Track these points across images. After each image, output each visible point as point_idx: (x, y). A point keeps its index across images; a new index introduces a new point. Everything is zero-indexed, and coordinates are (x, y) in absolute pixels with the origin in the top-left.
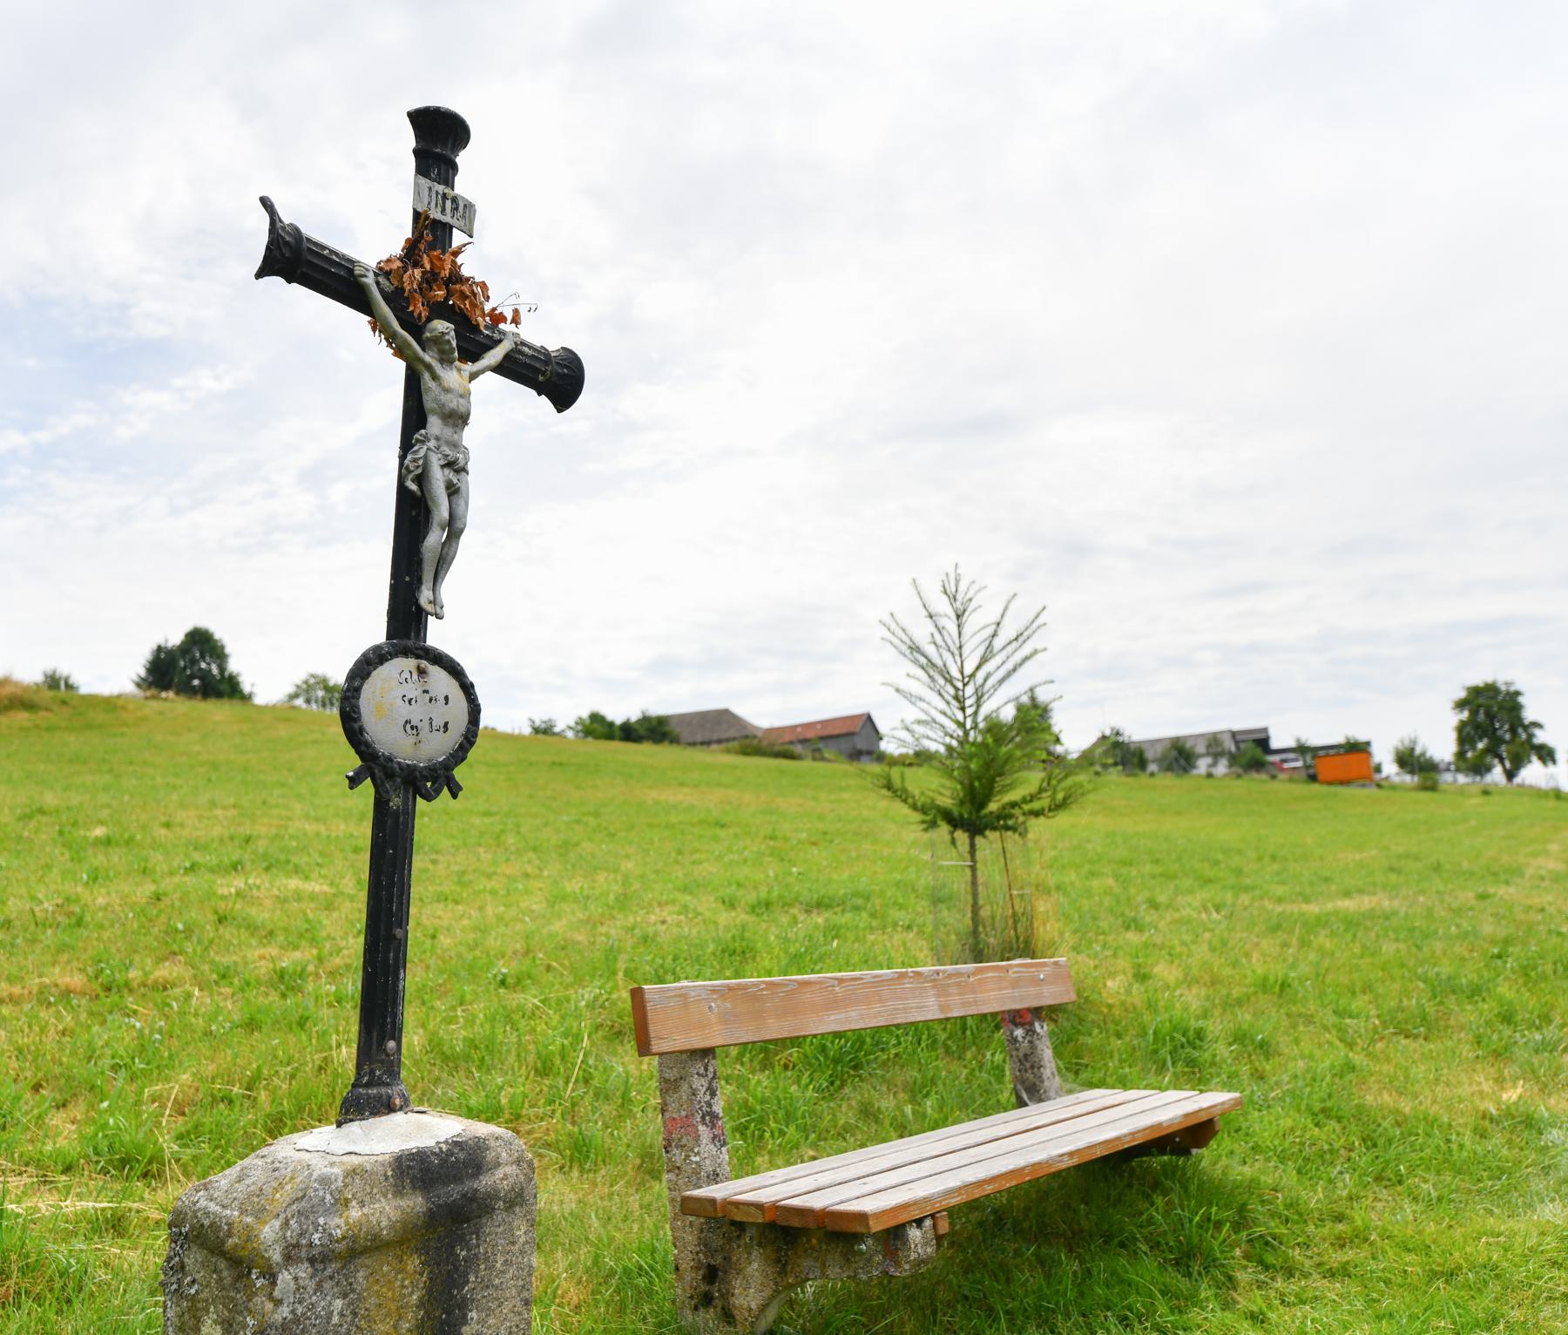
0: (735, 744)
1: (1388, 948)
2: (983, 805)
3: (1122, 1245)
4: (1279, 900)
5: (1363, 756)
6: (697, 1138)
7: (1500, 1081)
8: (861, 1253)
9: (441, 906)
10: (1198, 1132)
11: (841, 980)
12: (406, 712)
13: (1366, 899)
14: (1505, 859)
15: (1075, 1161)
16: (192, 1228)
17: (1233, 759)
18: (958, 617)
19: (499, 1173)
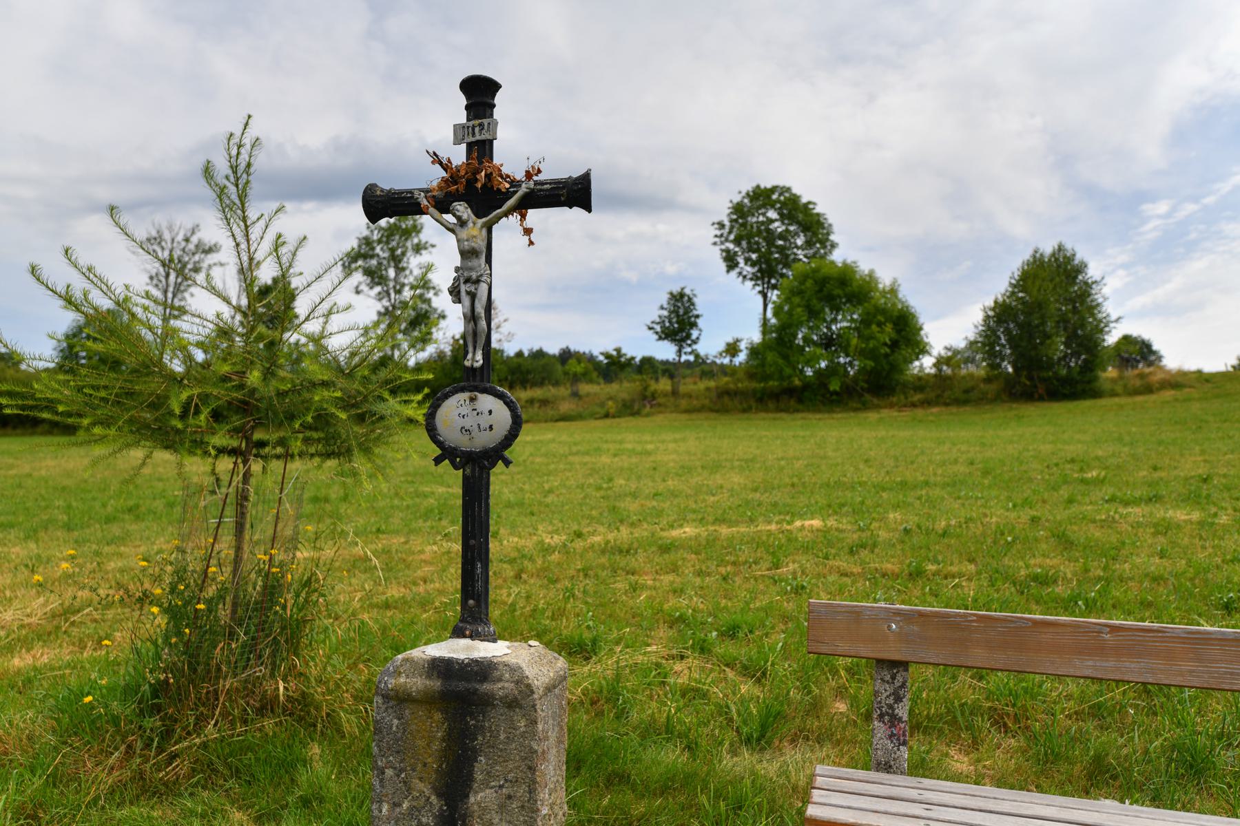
11: (1114, 629)
12: (462, 422)
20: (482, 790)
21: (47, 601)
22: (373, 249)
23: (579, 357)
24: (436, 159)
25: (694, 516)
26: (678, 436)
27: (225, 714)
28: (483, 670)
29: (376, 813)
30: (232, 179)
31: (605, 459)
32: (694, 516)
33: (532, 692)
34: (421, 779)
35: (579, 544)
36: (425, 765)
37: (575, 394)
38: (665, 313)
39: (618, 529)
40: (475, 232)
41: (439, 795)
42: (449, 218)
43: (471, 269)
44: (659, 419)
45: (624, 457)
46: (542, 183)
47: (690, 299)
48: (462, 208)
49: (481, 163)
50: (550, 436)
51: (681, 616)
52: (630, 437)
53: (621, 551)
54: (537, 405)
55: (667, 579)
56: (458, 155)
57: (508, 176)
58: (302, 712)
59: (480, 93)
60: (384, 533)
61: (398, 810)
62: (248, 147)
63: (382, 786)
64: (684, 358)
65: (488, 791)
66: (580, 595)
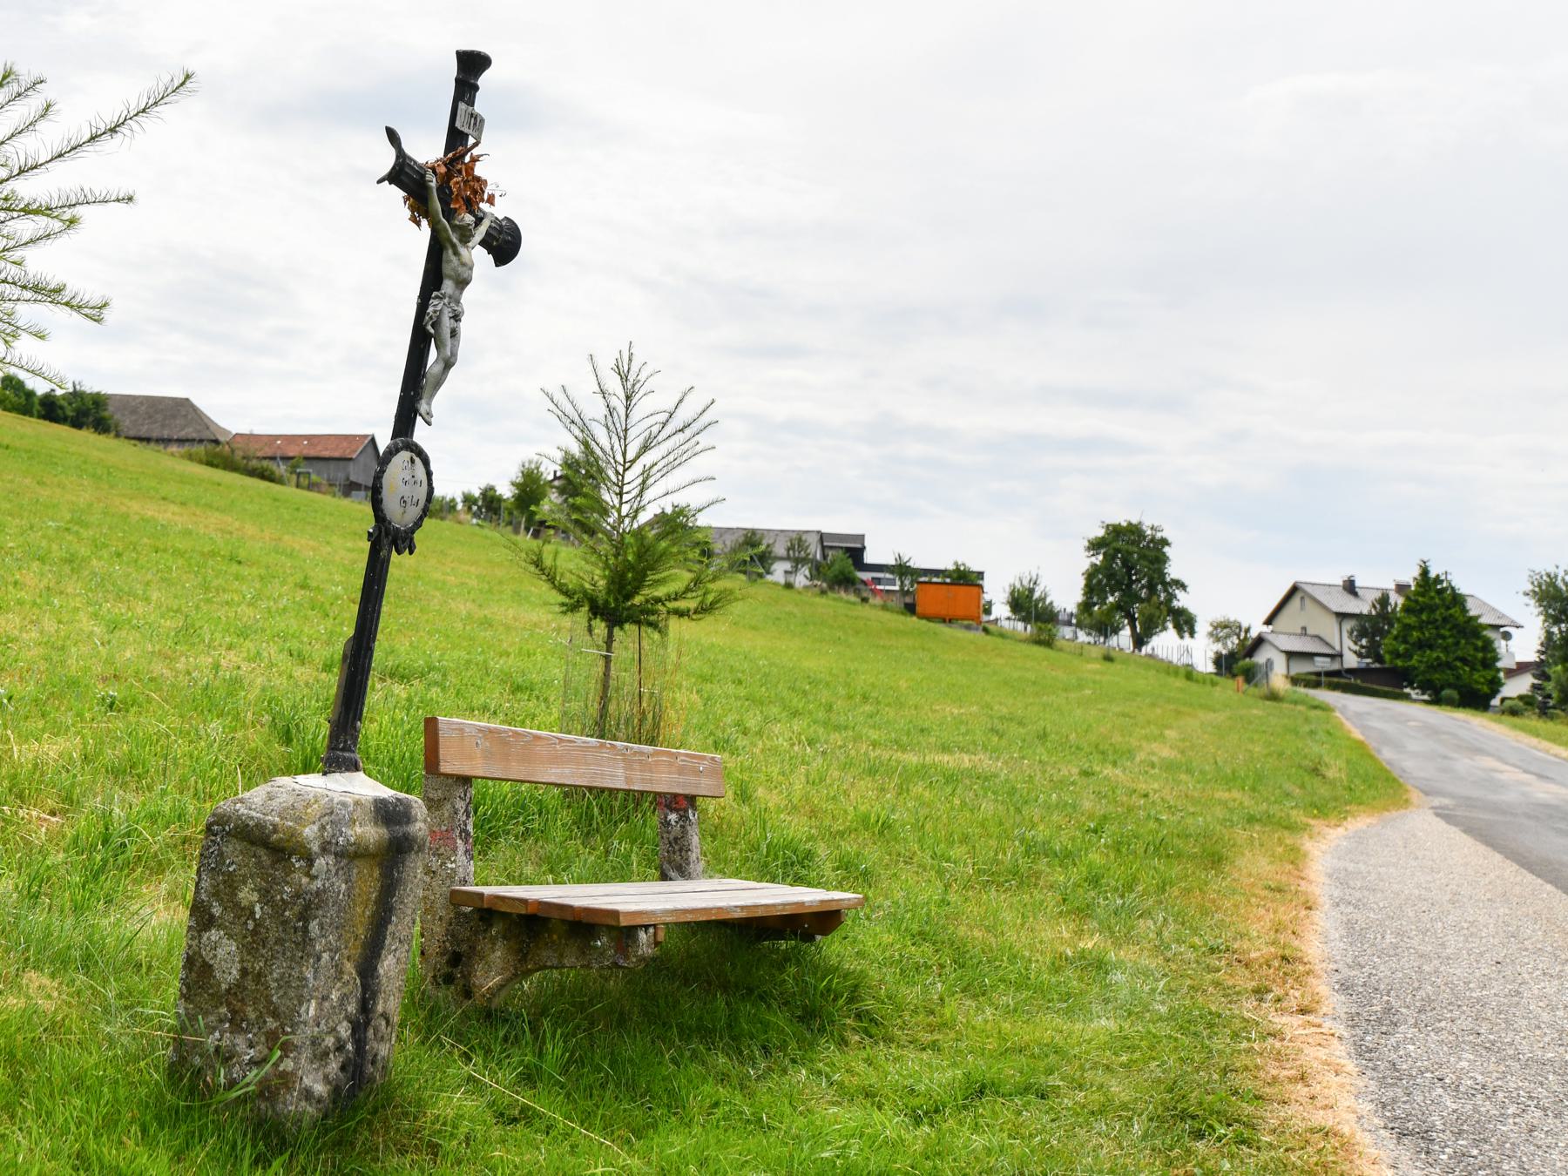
0: (200, 449)
1: (987, 807)
2: (628, 597)
3: (762, 998)
4: (874, 744)
5: (975, 589)
6: (455, 850)
7: (1079, 933)
8: (596, 947)
10: (826, 920)
13: (966, 758)
14: (1117, 738)
15: (743, 915)
16: (236, 827)
17: (817, 570)
18: (628, 398)
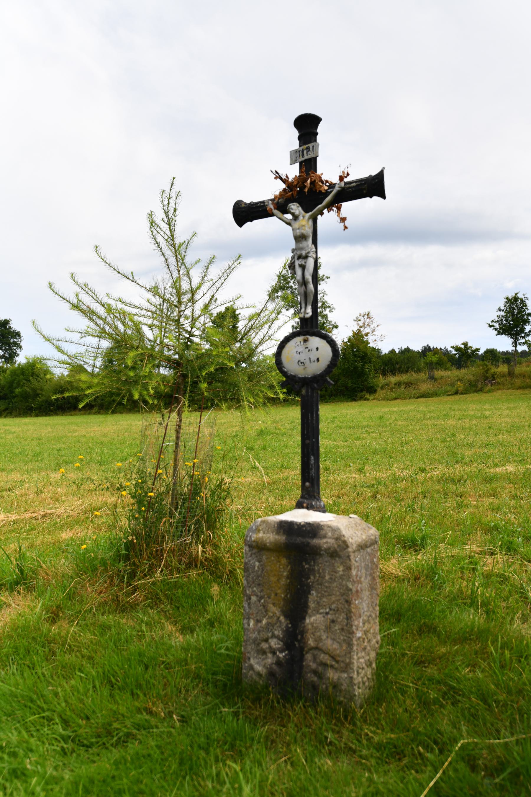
9: (38, 451)
12: (298, 357)
19: (324, 540)
20: (314, 615)
21: (83, 503)
22: (288, 283)
23: (436, 351)
24: (278, 176)
25: (515, 459)
26: (511, 405)
27: (167, 566)
28: (313, 530)
29: (246, 626)
30: (166, 220)
31: (452, 422)
32: (515, 459)
33: (347, 547)
34: (274, 604)
35: (421, 476)
36: (276, 594)
37: (432, 378)
38: (503, 314)
39: (453, 467)
40: (304, 222)
41: (286, 616)
42: (289, 216)
43: (302, 249)
44: (498, 394)
45: (467, 421)
46: (350, 183)
47: (523, 301)
48: (295, 207)
49: (308, 174)
50: (412, 407)
51: (495, 526)
52: (473, 406)
53: (453, 481)
54: (403, 386)
55: (486, 501)
56: (293, 172)
57: (327, 182)
58: (213, 567)
59: (307, 126)
60: (285, 468)
61: (259, 625)
62: (174, 198)
63: (250, 608)
64: (520, 348)
65: (318, 616)
66: (418, 510)
